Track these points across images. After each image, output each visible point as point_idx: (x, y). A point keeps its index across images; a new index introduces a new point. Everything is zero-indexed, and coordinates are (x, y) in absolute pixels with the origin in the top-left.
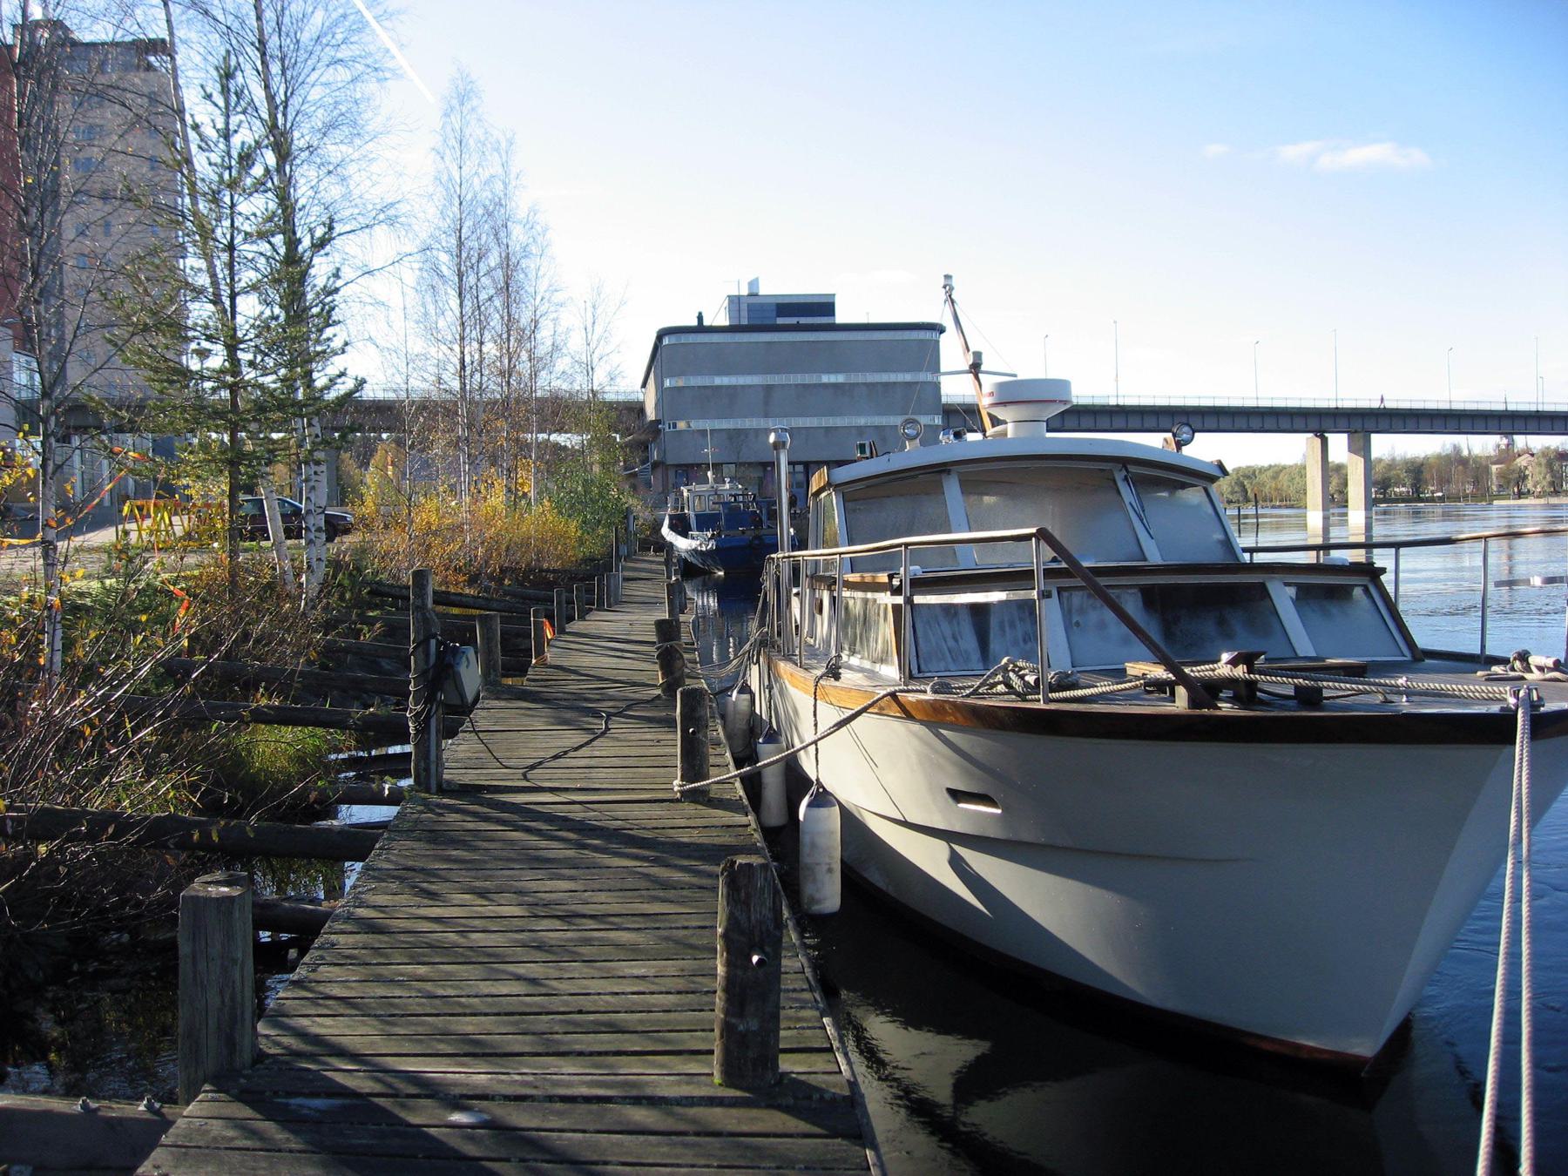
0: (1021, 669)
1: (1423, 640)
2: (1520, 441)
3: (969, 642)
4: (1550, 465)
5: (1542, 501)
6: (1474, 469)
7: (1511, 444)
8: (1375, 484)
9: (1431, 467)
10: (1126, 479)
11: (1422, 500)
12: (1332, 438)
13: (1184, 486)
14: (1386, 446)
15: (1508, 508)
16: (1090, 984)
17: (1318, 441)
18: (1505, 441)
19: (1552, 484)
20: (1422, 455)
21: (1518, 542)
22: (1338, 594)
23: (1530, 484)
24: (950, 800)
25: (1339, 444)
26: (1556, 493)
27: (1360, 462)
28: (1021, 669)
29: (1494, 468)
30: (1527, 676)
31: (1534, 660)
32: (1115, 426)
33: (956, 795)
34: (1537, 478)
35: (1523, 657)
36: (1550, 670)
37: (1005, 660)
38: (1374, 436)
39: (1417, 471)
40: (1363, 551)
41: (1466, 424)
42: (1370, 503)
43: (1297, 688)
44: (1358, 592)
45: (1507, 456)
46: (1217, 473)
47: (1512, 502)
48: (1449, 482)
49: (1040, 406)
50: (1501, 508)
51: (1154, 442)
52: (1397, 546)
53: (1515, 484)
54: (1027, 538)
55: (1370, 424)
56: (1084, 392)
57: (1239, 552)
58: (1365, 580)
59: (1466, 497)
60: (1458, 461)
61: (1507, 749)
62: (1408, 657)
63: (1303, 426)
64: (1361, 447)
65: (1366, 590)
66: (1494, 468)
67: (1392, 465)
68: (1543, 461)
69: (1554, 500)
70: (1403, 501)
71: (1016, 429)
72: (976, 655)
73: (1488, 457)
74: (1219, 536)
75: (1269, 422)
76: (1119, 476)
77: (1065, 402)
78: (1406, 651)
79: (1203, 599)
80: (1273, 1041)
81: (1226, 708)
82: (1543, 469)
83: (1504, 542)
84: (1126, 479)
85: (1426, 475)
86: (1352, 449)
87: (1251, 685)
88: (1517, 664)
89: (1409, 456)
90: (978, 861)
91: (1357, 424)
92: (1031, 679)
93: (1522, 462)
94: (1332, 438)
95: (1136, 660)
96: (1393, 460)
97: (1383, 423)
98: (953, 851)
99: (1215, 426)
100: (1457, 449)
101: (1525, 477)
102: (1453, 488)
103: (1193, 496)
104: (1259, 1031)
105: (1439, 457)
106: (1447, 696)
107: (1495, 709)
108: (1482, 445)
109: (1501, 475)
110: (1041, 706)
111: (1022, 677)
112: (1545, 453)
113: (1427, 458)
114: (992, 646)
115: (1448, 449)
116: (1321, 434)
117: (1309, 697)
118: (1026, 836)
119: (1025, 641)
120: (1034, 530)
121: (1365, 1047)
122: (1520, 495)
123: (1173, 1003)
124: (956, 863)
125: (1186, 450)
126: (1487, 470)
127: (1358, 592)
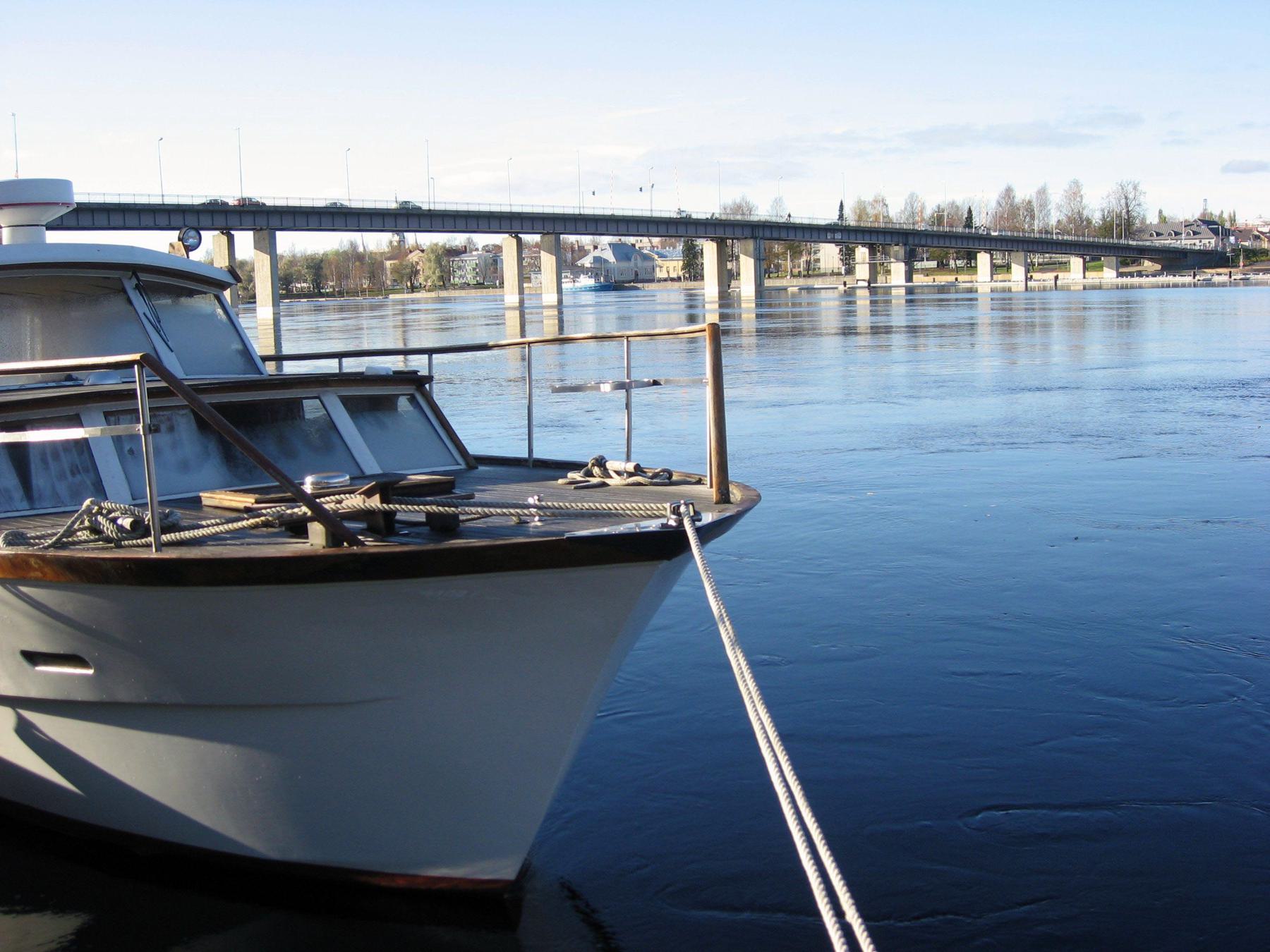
0: (110, 512)
1: (474, 449)
2: (411, 238)
3: (11, 480)
4: (438, 260)
5: (433, 295)
6: (370, 265)
7: (402, 241)
8: (280, 279)
9: (330, 264)
10: (137, 287)
11: (322, 295)
12: (238, 235)
13: (191, 293)
14: (292, 243)
15: (403, 302)
16: (170, 839)
17: (224, 239)
18: (396, 238)
19: (441, 278)
20: (321, 252)
21: (568, 347)
22: (383, 405)
23: (421, 279)
24: (25, 664)
25: (245, 241)
26: (444, 287)
27: (266, 258)
28: (110, 512)
29: (388, 264)
30: (608, 481)
31: (611, 465)
32: (112, 225)
33: (33, 658)
34: (428, 273)
35: (601, 462)
36: (631, 475)
37: (88, 502)
38: (278, 233)
39: (317, 267)
40: (401, 358)
41: (365, 222)
42: (277, 300)
43: (428, 514)
44: (403, 403)
45: (399, 252)
46: (228, 278)
47: (406, 296)
48: (347, 277)
49: (43, 208)
50: (396, 302)
51: (158, 243)
52: (430, 352)
53: (408, 278)
54: (129, 365)
55: (275, 221)
56: (86, 192)
57: (259, 362)
58: (410, 389)
59: (363, 291)
60: (355, 257)
61: (690, 565)
62: (463, 466)
63: (209, 223)
64: (266, 244)
65: (412, 399)
66: (388, 264)
67: (293, 262)
68: (433, 257)
69: (444, 294)
70: (305, 296)
71: (13, 236)
72: (18, 494)
73: (382, 254)
74: (237, 346)
75: (147, 219)
76: (130, 285)
77: (68, 205)
78: (460, 460)
79: (251, 419)
80: (393, 876)
81: (371, 544)
82: (433, 265)
83: (554, 348)
84: (137, 287)
85: (326, 271)
86: (258, 246)
87: (389, 515)
88: (596, 470)
89: (309, 252)
90: (52, 726)
91: (262, 221)
92: (126, 522)
93: (414, 257)
94: (238, 235)
95: (211, 489)
96: (294, 256)
97: (288, 221)
98: (21, 719)
99: (121, 223)
100: (353, 246)
101: (417, 272)
102: (351, 284)
103: (204, 304)
104: (377, 868)
105: (337, 253)
106: (616, 515)
107: (653, 525)
108: (376, 242)
109: (395, 270)
110: (153, 554)
111: (114, 520)
112: (434, 249)
113: (325, 255)
114: (34, 482)
115: (353, 246)
116: (227, 231)
117: (444, 526)
118: (123, 695)
119: (73, 474)
120: (137, 357)
121: (505, 869)
122: (413, 289)
123: (297, 854)
124: (26, 732)
125: (195, 256)
126: (382, 264)
127: (403, 403)
